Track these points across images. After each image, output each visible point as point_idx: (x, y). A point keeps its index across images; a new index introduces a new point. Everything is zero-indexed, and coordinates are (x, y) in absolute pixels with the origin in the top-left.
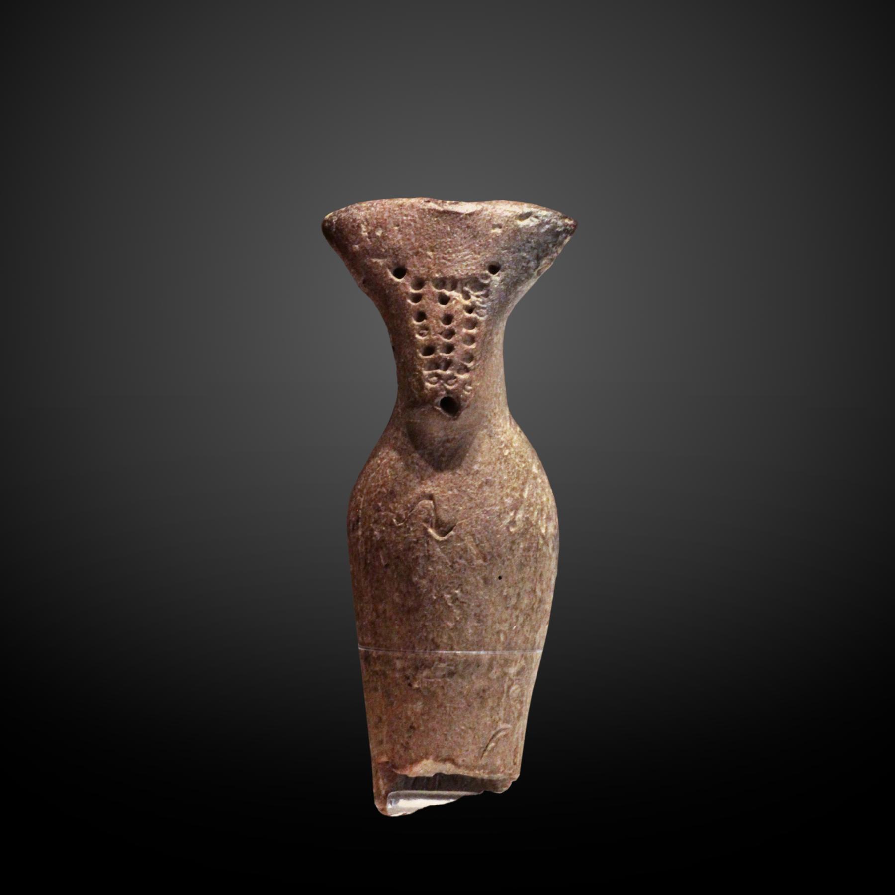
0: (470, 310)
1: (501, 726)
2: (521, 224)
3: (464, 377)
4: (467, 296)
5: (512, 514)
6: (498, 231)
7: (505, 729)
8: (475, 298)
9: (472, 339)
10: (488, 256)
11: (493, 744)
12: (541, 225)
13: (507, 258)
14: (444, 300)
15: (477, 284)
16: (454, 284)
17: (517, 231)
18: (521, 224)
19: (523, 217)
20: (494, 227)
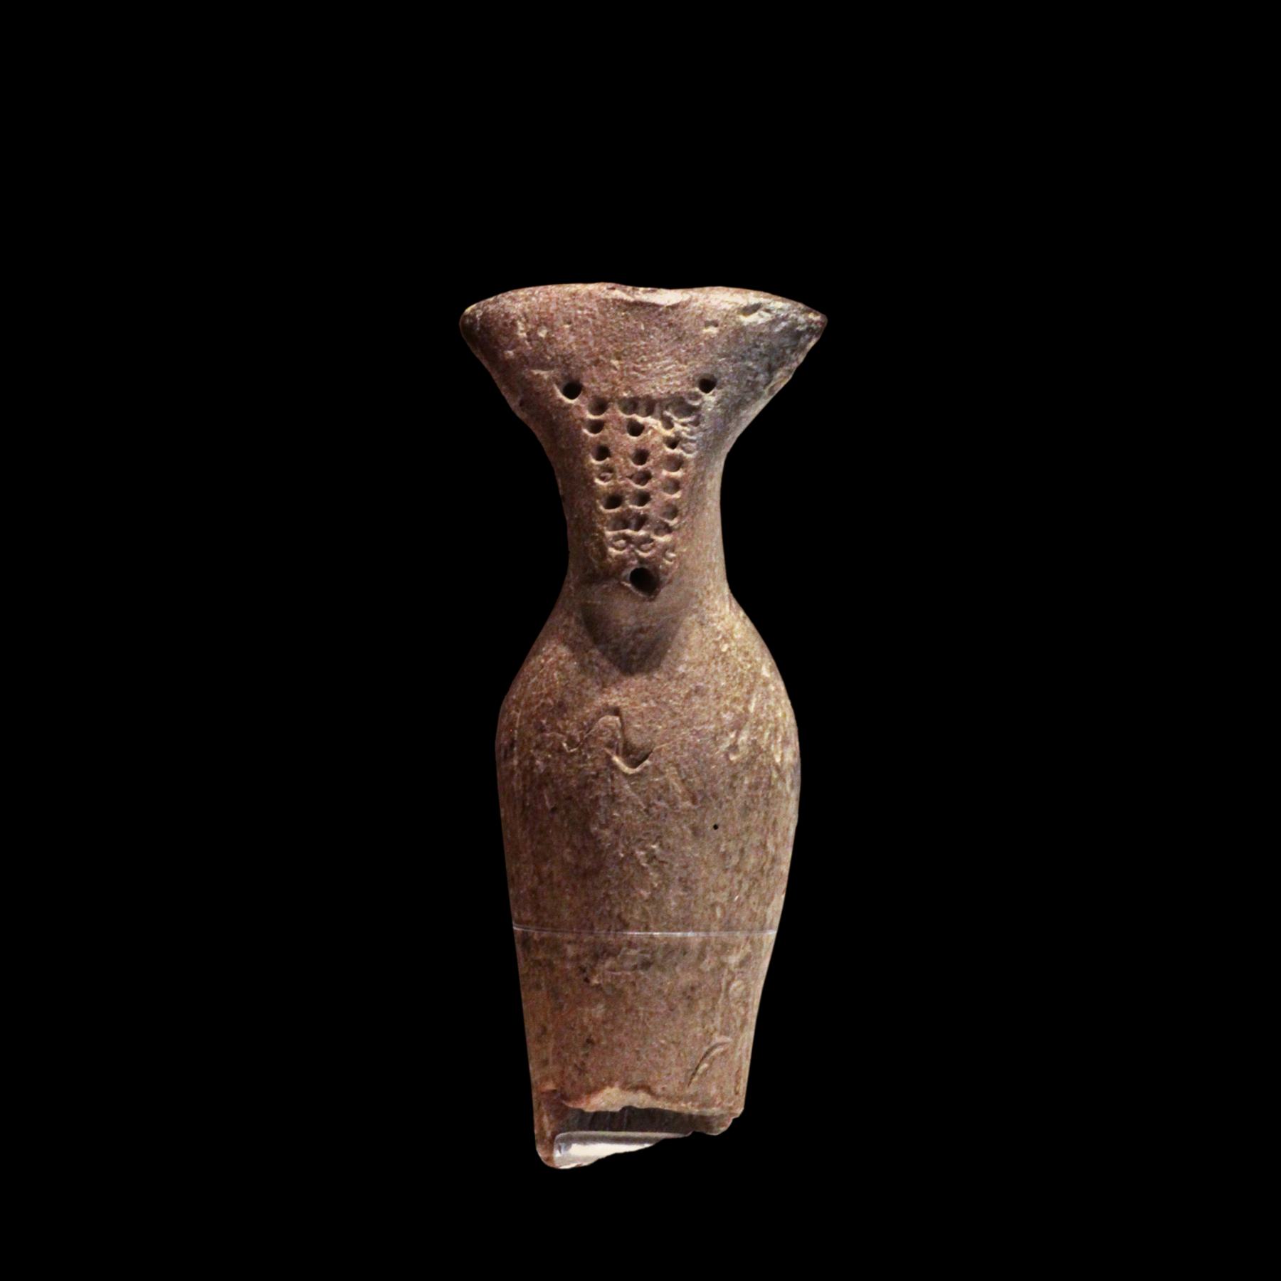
0: (673, 443)
1: (718, 1039)
2: (746, 320)
3: (664, 539)
4: (668, 424)
5: (732, 735)
6: (713, 331)
7: (722, 1044)
8: (681, 426)
9: (676, 485)
10: (698, 367)
11: (705, 1066)
12: (774, 322)
13: (726, 369)
14: (636, 429)
15: (683, 406)
16: (650, 406)
17: (740, 330)
18: (746, 320)
19: (748, 310)
20: (707, 324)
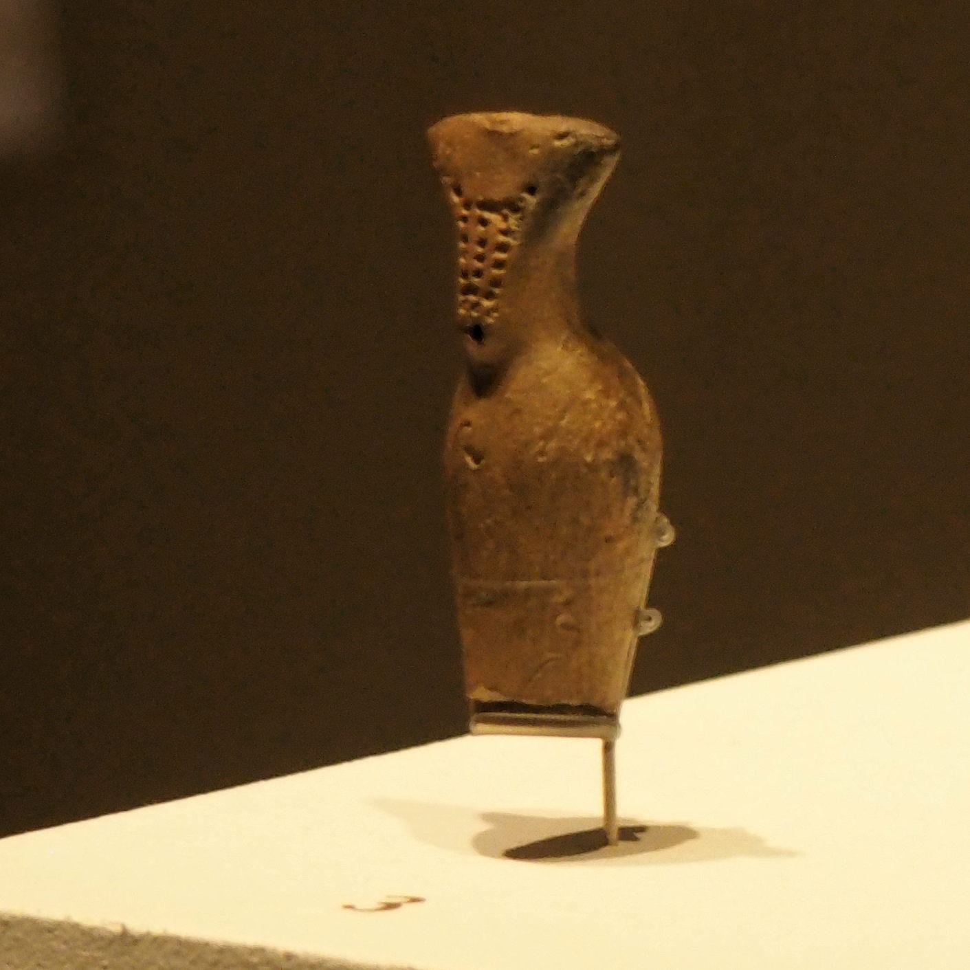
0: (505, 232)
1: (550, 655)
2: (557, 143)
3: (487, 303)
4: (505, 218)
5: (541, 443)
6: (535, 151)
7: (552, 659)
8: (513, 222)
9: (499, 264)
10: (521, 179)
11: (539, 675)
12: (576, 145)
13: (544, 180)
14: (484, 222)
15: (514, 206)
16: (488, 206)
17: (554, 151)
18: (557, 143)
19: (562, 136)
20: (533, 147)
